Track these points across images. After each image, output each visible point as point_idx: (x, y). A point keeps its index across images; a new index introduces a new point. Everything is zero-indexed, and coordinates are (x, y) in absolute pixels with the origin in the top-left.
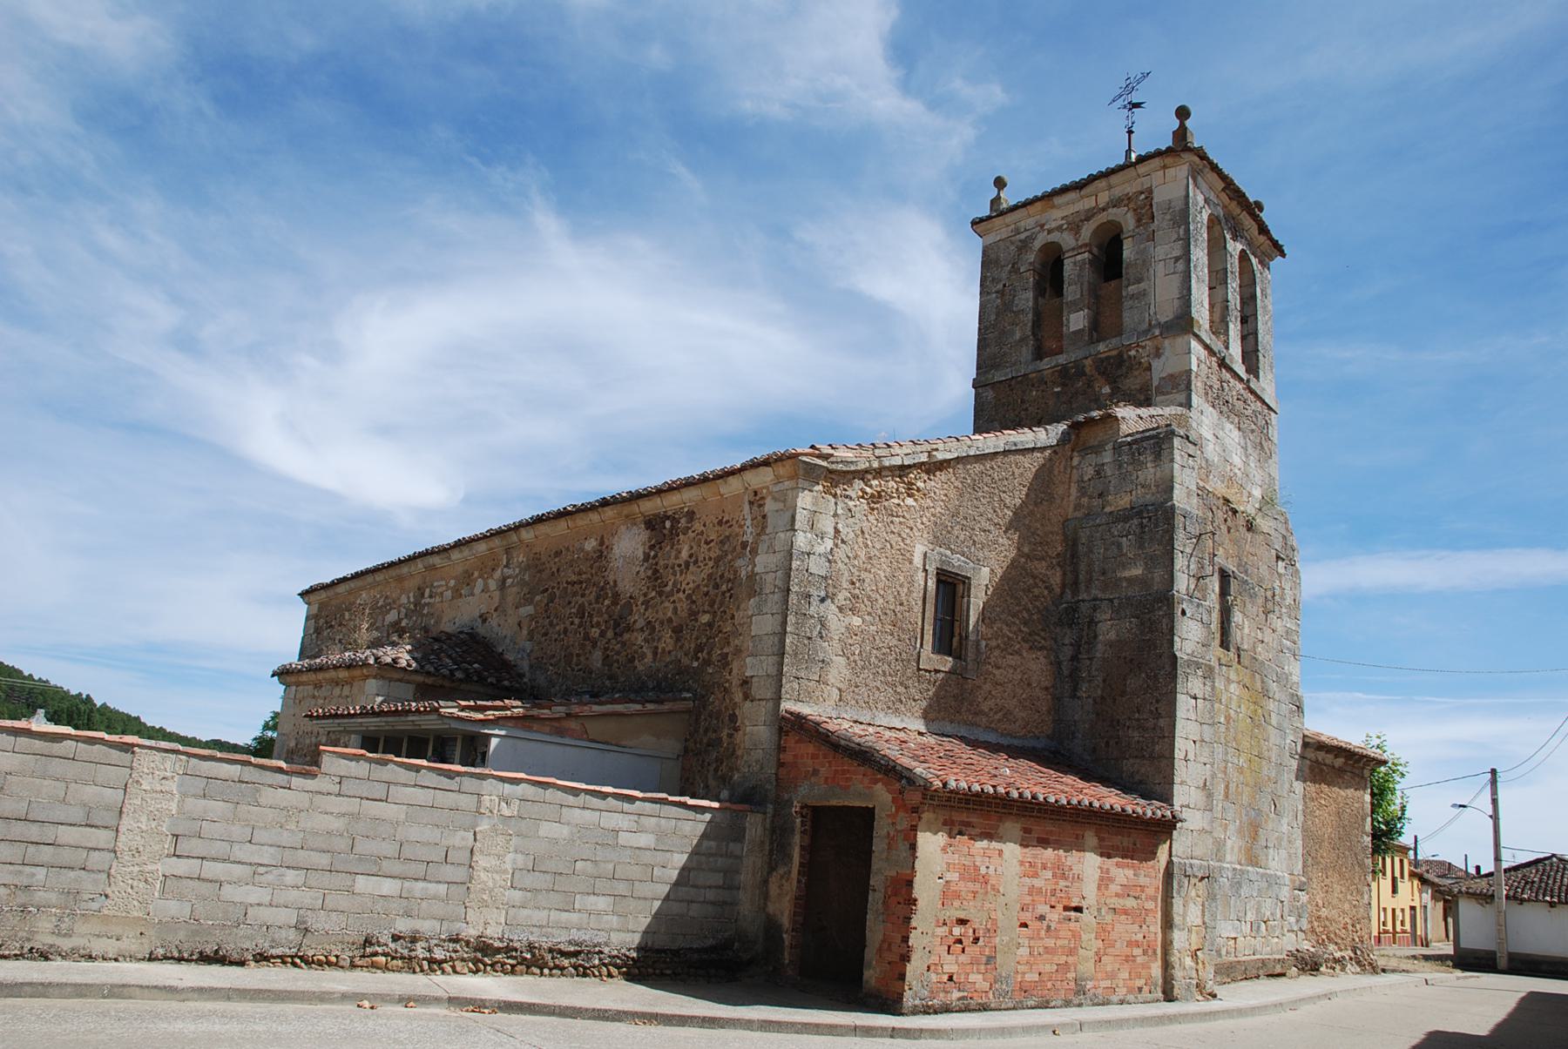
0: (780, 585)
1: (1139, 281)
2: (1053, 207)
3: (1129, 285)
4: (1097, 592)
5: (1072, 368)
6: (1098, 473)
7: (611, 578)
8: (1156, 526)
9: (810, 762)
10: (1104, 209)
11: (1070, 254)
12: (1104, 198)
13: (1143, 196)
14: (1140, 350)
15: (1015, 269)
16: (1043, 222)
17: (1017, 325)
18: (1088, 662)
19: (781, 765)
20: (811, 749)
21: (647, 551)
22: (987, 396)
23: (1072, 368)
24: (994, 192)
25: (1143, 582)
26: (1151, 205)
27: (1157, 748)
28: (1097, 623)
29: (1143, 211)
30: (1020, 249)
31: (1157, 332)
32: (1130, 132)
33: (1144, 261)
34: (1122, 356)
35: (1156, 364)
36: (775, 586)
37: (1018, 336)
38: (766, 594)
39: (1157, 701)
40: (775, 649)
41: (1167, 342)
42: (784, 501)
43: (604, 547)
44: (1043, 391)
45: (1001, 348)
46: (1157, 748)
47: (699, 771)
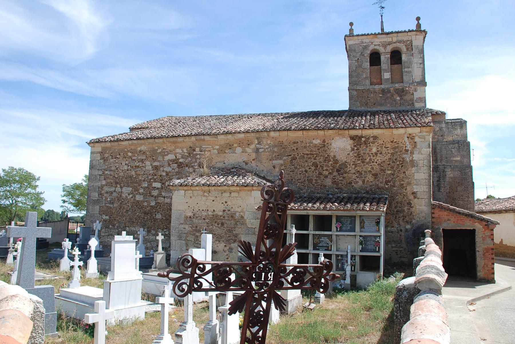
0: (426, 164)
1: (409, 68)
2: (377, 38)
3: (405, 68)
4: (444, 163)
5: (386, 90)
6: (440, 129)
7: (332, 154)
8: (464, 147)
9: (446, 217)
10: (395, 43)
11: (384, 54)
12: (395, 39)
13: (409, 42)
14: (410, 88)
15: (362, 54)
16: (372, 42)
17: (364, 72)
18: (444, 182)
19: (433, 218)
20: (446, 213)
21: (353, 147)
22: (354, 94)
23: (386, 90)
24: (350, 27)
25: (460, 162)
26: (412, 45)
27: (469, 206)
28: (446, 172)
29: (409, 47)
30: (364, 48)
31: (416, 84)
32: (382, 16)
33: (410, 62)
34: (403, 89)
35: (415, 93)
36: (424, 165)
37: (364, 76)
38: (420, 167)
39: (468, 194)
40: (427, 184)
41: (418, 88)
42: (424, 139)
43: (326, 143)
44: (375, 95)
45: (358, 79)
46: (469, 206)
47: (394, 220)
